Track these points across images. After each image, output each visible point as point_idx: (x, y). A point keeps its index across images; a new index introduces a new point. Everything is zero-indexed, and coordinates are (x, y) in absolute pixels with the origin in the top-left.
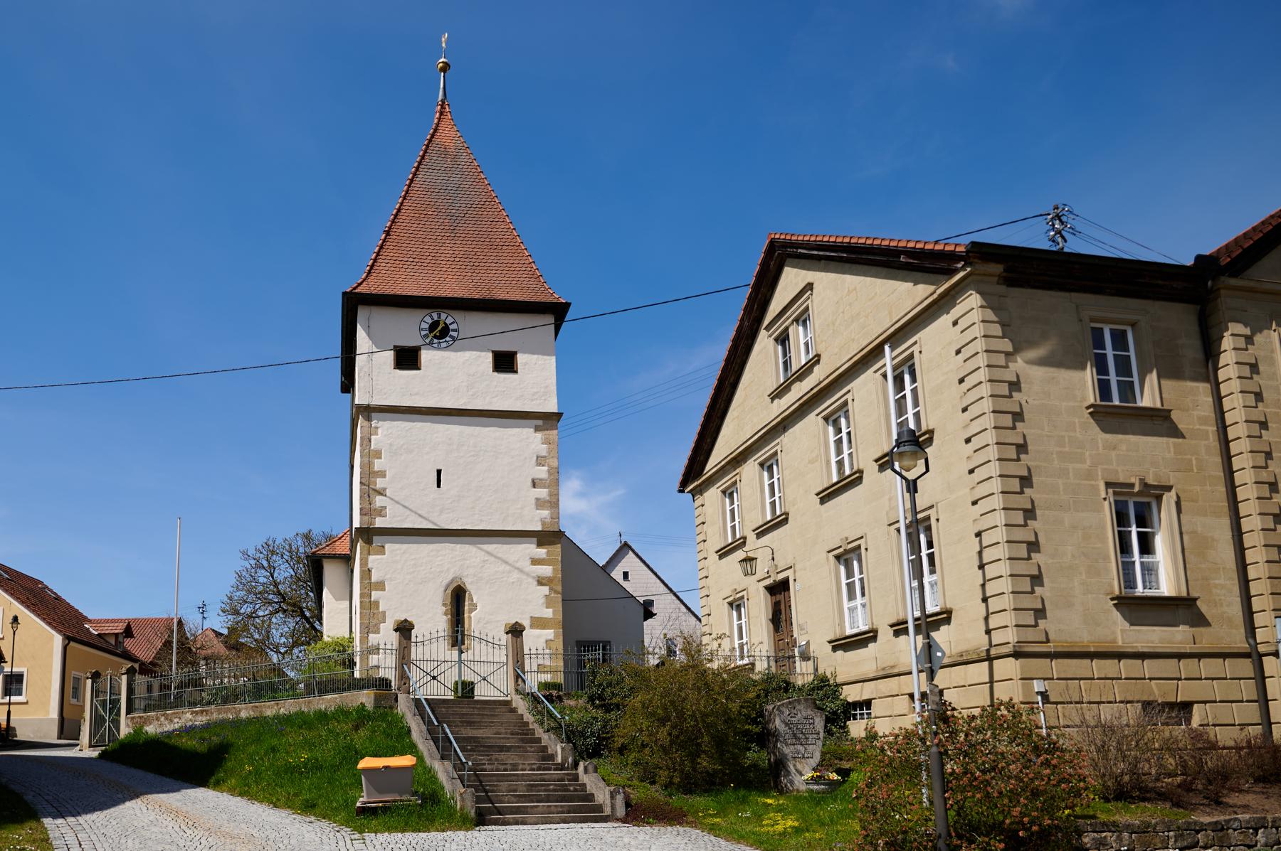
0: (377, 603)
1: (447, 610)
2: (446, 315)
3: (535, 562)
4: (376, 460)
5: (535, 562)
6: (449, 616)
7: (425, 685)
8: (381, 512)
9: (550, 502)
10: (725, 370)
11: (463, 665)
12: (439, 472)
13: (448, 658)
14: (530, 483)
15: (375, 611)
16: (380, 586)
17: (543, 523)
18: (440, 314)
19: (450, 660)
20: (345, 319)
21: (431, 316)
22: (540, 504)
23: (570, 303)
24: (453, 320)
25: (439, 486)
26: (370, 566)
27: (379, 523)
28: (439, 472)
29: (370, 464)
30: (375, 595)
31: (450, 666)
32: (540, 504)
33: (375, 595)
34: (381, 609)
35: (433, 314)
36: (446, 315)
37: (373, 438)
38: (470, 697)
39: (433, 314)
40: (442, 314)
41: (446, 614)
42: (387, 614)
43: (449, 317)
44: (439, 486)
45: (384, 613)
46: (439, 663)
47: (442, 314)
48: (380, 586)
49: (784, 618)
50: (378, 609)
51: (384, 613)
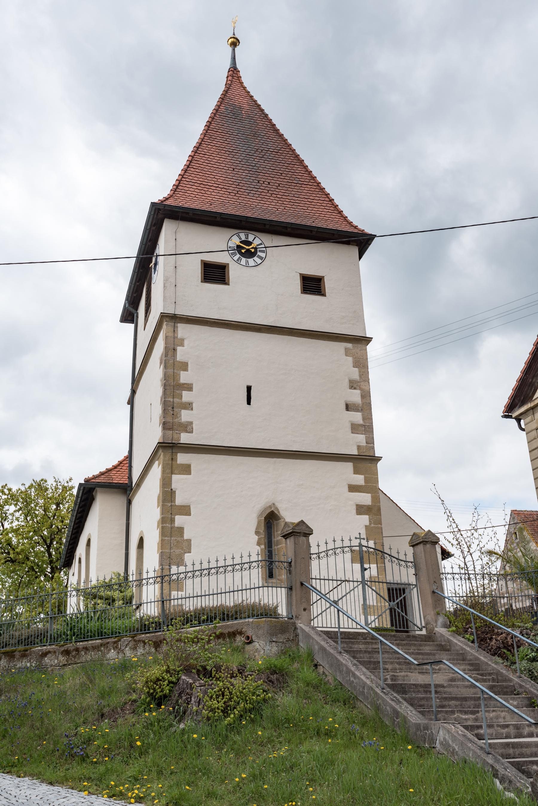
0: (181, 530)
1: (259, 539)
2: (254, 237)
3: (353, 488)
4: (182, 372)
5: (353, 488)
6: (263, 547)
7: (324, 614)
8: (187, 427)
9: (364, 426)
10: (142, 562)
11: (366, 586)
12: (249, 389)
13: (349, 576)
14: (344, 407)
15: (179, 539)
16: (185, 510)
17: (359, 447)
19: (335, 578)
20: (147, 234)
22: (355, 428)
23: (324, 295)
24: (260, 242)
25: (249, 402)
26: (174, 486)
27: (185, 438)
28: (249, 389)
29: (176, 377)
30: (179, 520)
31: (335, 585)
32: (355, 428)
33: (179, 520)
34: (186, 537)
36: (254, 237)
37: (179, 349)
38: (407, 632)
39: (240, 234)
40: (250, 235)
41: (259, 544)
42: (192, 542)
43: (257, 238)
44: (249, 402)
45: (189, 541)
46: (339, 582)
47: (250, 235)
48: (185, 510)
49: (404, 585)
50: (183, 536)
51: (189, 541)
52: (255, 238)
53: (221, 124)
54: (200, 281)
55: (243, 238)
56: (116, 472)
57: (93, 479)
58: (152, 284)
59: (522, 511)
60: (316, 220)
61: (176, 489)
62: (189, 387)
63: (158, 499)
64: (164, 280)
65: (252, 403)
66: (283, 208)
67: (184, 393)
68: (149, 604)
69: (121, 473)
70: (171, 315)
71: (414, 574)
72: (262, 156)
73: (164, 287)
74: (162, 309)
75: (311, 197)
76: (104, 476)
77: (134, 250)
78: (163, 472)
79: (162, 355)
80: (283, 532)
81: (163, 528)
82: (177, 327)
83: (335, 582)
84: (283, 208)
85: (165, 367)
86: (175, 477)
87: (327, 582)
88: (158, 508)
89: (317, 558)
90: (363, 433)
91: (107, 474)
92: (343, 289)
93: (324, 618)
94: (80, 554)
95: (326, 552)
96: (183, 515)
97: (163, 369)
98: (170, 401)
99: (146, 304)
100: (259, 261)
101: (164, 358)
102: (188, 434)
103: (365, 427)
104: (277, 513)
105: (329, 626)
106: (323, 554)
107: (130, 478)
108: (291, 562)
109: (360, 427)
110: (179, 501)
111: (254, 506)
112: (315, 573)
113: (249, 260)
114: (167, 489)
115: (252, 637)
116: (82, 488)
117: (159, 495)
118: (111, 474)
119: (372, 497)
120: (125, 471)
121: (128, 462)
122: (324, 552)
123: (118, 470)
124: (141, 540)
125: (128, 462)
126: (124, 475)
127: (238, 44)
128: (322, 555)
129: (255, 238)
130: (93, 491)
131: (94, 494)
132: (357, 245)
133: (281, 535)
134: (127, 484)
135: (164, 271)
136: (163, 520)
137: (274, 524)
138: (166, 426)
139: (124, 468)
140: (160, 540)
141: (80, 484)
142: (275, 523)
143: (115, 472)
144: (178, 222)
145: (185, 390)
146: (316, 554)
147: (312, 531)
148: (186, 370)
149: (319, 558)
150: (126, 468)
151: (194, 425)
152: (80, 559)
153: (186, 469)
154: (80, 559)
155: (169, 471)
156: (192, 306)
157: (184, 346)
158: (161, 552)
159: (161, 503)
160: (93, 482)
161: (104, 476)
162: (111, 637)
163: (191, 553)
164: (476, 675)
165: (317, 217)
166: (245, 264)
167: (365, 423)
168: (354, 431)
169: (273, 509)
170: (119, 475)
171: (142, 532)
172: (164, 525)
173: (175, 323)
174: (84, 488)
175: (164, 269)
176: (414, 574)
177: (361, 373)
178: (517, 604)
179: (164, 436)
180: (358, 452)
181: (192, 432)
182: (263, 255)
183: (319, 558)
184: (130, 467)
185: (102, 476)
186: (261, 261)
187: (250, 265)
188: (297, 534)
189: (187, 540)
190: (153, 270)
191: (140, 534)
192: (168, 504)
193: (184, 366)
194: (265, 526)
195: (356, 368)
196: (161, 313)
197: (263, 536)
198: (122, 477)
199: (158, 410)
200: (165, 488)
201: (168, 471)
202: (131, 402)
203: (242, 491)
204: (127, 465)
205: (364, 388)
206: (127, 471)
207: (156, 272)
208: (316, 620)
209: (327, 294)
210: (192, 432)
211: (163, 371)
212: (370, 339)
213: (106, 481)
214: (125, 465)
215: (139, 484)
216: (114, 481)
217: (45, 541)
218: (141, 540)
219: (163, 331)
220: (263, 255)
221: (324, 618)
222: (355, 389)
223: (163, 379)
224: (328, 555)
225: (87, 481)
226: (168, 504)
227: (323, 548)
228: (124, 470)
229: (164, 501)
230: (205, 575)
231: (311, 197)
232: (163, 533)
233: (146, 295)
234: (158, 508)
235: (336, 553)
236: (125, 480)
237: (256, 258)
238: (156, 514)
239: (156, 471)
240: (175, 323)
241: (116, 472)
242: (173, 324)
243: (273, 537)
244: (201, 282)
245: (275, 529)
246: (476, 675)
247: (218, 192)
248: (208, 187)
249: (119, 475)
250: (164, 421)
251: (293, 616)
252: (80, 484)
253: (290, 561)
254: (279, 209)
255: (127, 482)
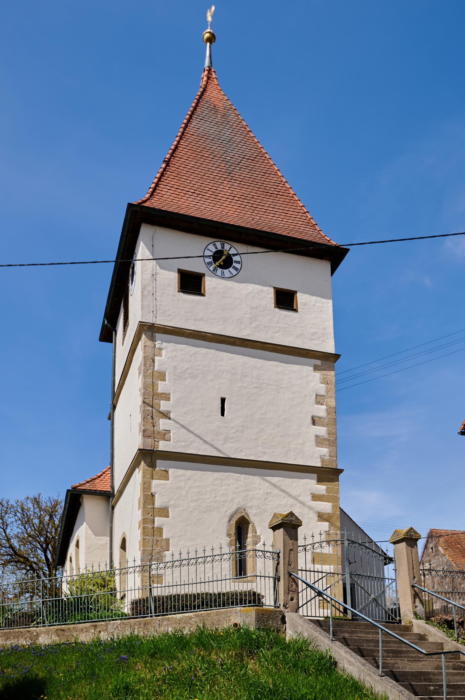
0: (160, 530)
2: (230, 246)
4: (160, 382)
5: (316, 497)
9: (329, 440)
12: (223, 401)
14: (310, 421)
17: (323, 461)
18: (224, 244)
21: (215, 245)
25: (223, 414)
27: (162, 446)
28: (223, 401)
31: (320, 577)
34: (164, 537)
35: (216, 243)
37: (157, 358)
39: (216, 243)
40: (226, 245)
41: (230, 544)
42: (170, 541)
43: (232, 248)
44: (223, 414)
45: (168, 540)
46: (324, 574)
51: (168, 540)
52: (231, 248)
53: (196, 127)
54: (177, 290)
55: (219, 248)
56: (99, 481)
57: (79, 486)
58: (130, 296)
59: (439, 530)
60: (291, 232)
61: (156, 493)
62: (166, 397)
63: (139, 502)
64: (142, 288)
65: (225, 415)
66: (259, 218)
67: (162, 402)
68: (137, 591)
69: (104, 482)
70: (149, 324)
71: (394, 570)
72: (238, 163)
73: (142, 295)
74: (141, 317)
75: (286, 209)
76: (90, 484)
77: (112, 253)
78: (144, 477)
79: (141, 365)
80: (271, 523)
81: (144, 528)
82: (155, 337)
83: (320, 574)
84: (259, 218)
85: (145, 377)
86: (155, 482)
87: (312, 573)
88: (139, 510)
89: (304, 550)
90: (328, 446)
91: (91, 483)
92: (314, 305)
93: (309, 608)
94: (71, 553)
95: (320, 543)
96: (162, 517)
97: (142, 379)
98: (149, 410)
99: (124, 319)
100: (234, 272)
101: (143, 368)
102: (166, 442)
103: (329, 441)
104: (247, 518)
105: (314, 615)
106: (317, 545)
107: (113, 487)
108: (280, 552)
109: (325, 441)
110: (157, 504)
111: (227, 511)
112: (301, 565)
113: (225, 271)
114: (148, 493)
115: (240, 625)
116: (69, 495)
117: (140, 498)
118: (95, 483)
119: (333, 505)
120: (108, 480)
121: (110, 472)
122: (311, 544)
123: (101, 479)
124: (124, 540)
125: (110, 472)
126: (107, 484)
127: (213, 40)
128: (308, 548)
129: (231, 248)
130: (80, 498)
131: (80, 500)
132: (329, 260)
133: (270, 527)
134: (109, 491)
135: (142, 278)
136: (144, 521)
137: (244, 528)
138: (145, 434)
139: (106, 477)
140: (142, 539)
141: (68, 490)
142: (244, 527)
143: (99, 481)
144: (155, 227)
145: (163, 400)
146: (303, 546)
147: (301, 522)
148: (164, 380)
149: (305, 550)
150: (108, 478)
151: (171, 434)
152: (71, 558)
153: (165, 475)
154: (71, 558)
155: (149, 476)
156: (169, 316)
157: (161, 356)
158: (143, 550)
159: (142, 506)
160: (80, 489)
161: (90, 484)
162: (101, 621)
163: (169, 551)
164: (459, 664)
165: (292, 229)
166: (220, 275)
167: (329, 437)
168: (318, 445)
169: (243, 514)
170: (102, 483)
171: (124, 533)
172: (145, 525)
173: (152, 332)
174: (72, 494)
175: (142, 276)
176: (394, 570)
177: (328, 390)
178: (325, 611)
179: (144, 443)
180: (322, 464)
181: (170, 440)
182: (238, 266)
183: (305, 550)
184: (112, 476)
185: (87, 484)
186: (236, 273)
187: (225, 276)
188: (286, 525)
189: (166, 539)
190: (130, 282)
191: (123, 535)
192: (148, 506)
193: (162, 376)
194: (235, 529)
195: (324, 384)
196: (140, 322)
197: (234, 538)
198: (105, 486)
199: (138, 418)
200: (145, 492)
201: (148, 476)
202: (111, 418)
203: (215, 497)
204: (109, 475)
205: (330, 404)
206: (110, 480)
207: (134, 282)
208: (301, 609)
209: (299, 310)
210: (170, 440)
211: (142, 381)
212: (339, 356)
213: (91, 488)
214: (107, 475)
215: (121, 492)
216: (98, 489)
217: (41, 546)
218: (124, 540)
219: (142, 343)
220: (238, 266)
221: (309, 608)
222: (322, 404)
223: (142, 389)
224: (315, 547)
225: (74, 488)
226: (148, 506)
227: (309, 541)
228: (106, 480)
229: (145, 503)
230: (192, 564)
231: (286, 209)
232: (145, 532)
233: (124, 316)
234: (139, 510)
235: (322, 546)
236: (108, 488)
237: (231, 269)
238: (138, 515)
239: (138, 475)
240: (152, 332)
241: (99, 481)
242: (151, 333)
243: (242, 539)
244: (178, 292)
245: (245, 533)
246: (459, 664)
247: (194, 197)
248: (184, 192)
249: (102, 483)
250: (143, 429)
251: (280, 605)
252: (68, 490)
253: (278, 551)
254: (254, 219)
255: (109, 490)
